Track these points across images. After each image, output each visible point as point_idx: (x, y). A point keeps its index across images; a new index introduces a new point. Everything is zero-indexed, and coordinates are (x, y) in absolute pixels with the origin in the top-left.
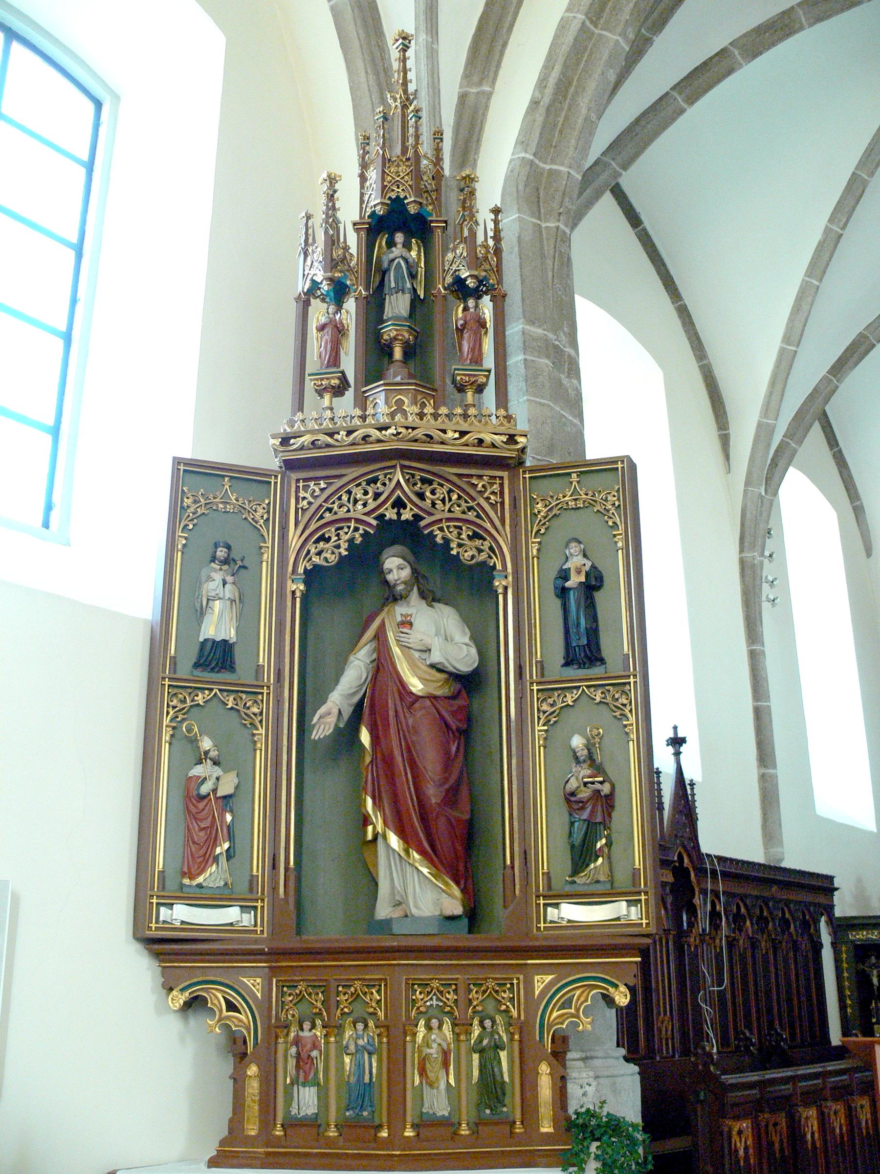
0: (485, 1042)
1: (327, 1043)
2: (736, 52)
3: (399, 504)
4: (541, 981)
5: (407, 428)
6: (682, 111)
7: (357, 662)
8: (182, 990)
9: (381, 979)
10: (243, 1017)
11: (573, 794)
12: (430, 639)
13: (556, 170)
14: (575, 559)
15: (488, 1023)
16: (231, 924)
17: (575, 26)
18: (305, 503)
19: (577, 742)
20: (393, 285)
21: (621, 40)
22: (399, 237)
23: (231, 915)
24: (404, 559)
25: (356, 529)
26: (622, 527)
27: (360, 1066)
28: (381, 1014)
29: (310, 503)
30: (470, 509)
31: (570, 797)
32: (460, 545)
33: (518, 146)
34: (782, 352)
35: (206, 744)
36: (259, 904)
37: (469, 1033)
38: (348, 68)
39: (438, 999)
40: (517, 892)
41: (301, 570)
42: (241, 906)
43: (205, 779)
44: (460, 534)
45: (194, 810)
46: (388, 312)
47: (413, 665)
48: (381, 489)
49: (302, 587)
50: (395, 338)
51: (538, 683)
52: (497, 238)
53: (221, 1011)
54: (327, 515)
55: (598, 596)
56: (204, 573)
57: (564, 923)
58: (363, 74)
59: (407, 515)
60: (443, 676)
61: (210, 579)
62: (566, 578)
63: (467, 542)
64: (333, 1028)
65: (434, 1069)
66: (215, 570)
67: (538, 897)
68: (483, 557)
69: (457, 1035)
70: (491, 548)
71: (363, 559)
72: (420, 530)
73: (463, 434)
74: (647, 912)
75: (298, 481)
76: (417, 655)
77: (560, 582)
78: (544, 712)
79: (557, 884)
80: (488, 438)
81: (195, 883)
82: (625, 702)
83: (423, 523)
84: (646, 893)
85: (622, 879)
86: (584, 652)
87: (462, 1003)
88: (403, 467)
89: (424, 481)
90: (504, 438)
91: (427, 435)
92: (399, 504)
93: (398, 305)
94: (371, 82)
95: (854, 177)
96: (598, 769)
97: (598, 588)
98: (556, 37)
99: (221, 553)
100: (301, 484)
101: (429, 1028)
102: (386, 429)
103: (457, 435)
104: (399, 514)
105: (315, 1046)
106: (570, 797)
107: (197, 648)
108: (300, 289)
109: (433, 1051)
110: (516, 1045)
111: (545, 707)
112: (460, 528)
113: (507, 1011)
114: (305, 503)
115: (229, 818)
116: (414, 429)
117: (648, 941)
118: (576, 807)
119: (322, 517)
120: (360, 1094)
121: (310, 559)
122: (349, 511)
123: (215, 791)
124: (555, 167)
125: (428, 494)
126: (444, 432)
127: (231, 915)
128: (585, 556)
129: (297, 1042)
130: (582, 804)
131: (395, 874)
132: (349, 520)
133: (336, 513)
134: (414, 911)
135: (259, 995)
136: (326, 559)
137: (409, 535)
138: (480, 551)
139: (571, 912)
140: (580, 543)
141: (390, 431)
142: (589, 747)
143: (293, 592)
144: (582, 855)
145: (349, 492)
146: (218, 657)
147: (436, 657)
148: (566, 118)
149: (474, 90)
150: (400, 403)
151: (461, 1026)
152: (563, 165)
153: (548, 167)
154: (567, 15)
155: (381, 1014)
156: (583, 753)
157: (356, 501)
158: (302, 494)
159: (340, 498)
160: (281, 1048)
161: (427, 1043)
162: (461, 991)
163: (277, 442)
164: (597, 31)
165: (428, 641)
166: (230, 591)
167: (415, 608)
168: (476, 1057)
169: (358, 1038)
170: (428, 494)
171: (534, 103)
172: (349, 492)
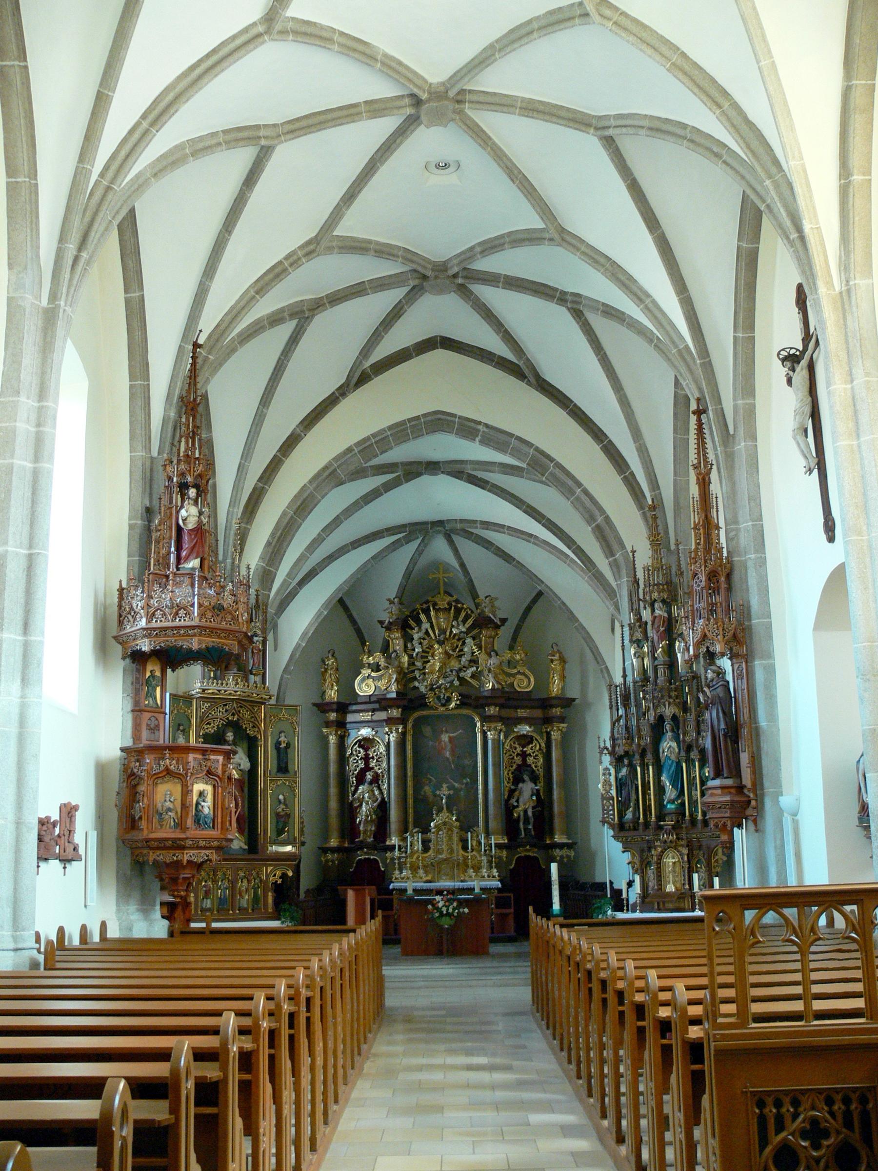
3: (233, 715)
4: (270, 869)
19: (281, 797)
27: (225, 893)
31: (278, 815)
52: (257, 600)
55: (289, 750)
64: (215, 881)
65: (243, 894)
80: (264, 696)
86: (283, 768)
92: (233, 715)
95: (337, 517)
99: (181, 728)
109: (244, 888)
120: (222, 901)
129: (204, 886)
130: (282, 816)
137: (235, 726)
139: (275, 848)
142: (285, 799)
144: (280, 832)
147: (242, 767)
151: (249, 881)
161: (241, 886)
165: (240, 761)
171: (268, 544)
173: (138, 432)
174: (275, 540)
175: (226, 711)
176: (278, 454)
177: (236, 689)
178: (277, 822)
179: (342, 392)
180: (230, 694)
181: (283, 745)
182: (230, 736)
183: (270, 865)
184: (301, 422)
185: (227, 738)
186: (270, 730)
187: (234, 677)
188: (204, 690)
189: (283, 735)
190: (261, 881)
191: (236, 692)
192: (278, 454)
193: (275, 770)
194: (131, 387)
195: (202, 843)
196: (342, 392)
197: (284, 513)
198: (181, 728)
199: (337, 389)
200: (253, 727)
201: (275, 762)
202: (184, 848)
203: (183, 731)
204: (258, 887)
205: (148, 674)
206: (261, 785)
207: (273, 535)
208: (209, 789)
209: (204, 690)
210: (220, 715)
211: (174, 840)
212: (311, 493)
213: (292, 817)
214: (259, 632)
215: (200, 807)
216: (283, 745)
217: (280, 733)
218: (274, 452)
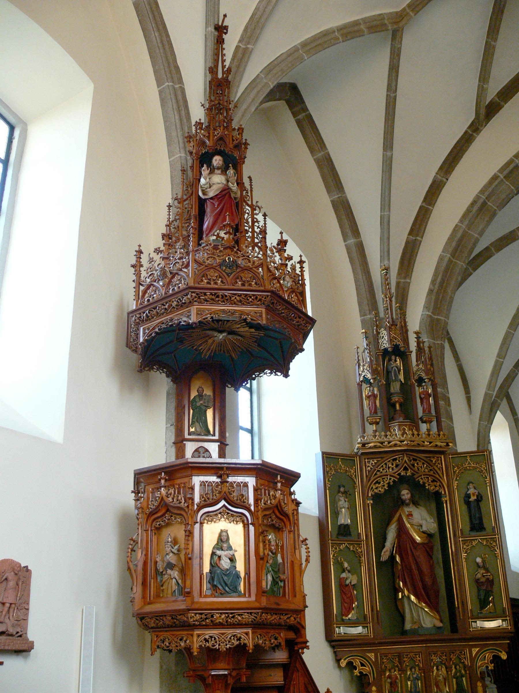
0: (458, 674)
1: (401, 677)
2: (493, 249)
3: (406, 469)
4: (475, 651)
5: (411, 441)
6: (471, 274)
7: (392, 530)
8: (345, 659)
9: (419, 652)
10: (367, 668)
11: (478, 579)
12: (419, 521)
13: (440, 319)
14: (471, 490)
15: (458, 667)
16: (360, 633)
17: (446, 259)
18: (369, 468)
19: (479, 560)
20: (394, 378)
21: (464, 265)
22: (393, 358)
23: (359, 630)
24: (408, 490)
25: (390, 479)
26: (488, 478)
27: (416, 686)
28: (421, 665)
29: (371, 468)
30: (431, 470)
32: (429, 485)
33: (425, 309)
34: (497, 362)
35: (346, 565)
36: (369, 625)
37: (451, 671)
38: (353, 271)
39: (440, 659)
40: (461, 617)
41: (370, 495)
42: (362, 626)
43: (347, 578)
44: (428, 480)
45: (344, 591)
46: (392, 390)
47: (416, 532)
48: (399, 463)
49: (372, 502)
50: (397, 401)
51: (462, 538)
53: (359, 667)
54: (378, 473)
55: (482, 504)
56: (337, 497)
57: (479, 629)
58: (361, 275)
59: (409, 474)
60: (426, 535)
61: (339, 500)
62: (470, 497)
63: (431, 483)
64: (402, 671)
65: (441, 685)
66: (341, 497)
67: (469, 619)
68: (437, 489)
69: (447, 672)
70: (440, 485)
71: (393, 489)
72: (414, 479)
73: (430, 443)
74: (510, 624)
75: (365, 459)
76: (416, 527)
77: (467, 499)
78: (465, 549)
79: (475, 614)
80: (439, 444)
81: (347, 618)
82: (495, 544)
83: (415, 476)
84: (509, 617)
85: (499, 611)
87: (448, 660)
88: (406, 454)
89: (414, 460)
90: (445, 444)
91: (418, 444)
92: (406, 469)
93: (395, 387)
94: (364, 279)
96: (487, 571)
97: (481, 501)
98: (438, 263)
99: (342, 489)
100: (366, 460)
101: (437, 669)
102: (403, 441)
103: (428, 443)
104: (406, 473)
105: (397, 678)
106: (477, 581)
107: (337, 528)
108: (358, 381)
109: (441, 678)
110: (468, 675)
111: (465, 547)
112: (428, 478)
113: (464, 662)
114: (369, 468)
115: (355, 592)
116: (413, 441)
117: (512, 635)
118: (481, 584)
119: (376, 474)
121: (373, 490)
122: (387, 472)
123: (351, 583)
124: (439, 317)
125: (416, 465)
126: (424, 442)
127: (359, 630)
128: (475, 488)
129: (389, 677)
131: (413, 611)
132: (387, 475)
133: (381, 472)
134: (424, 625)
135: (374, 660)
136: (380, 491)
138: (436, 486)
140: (473, 483)
141: (404, 443)
142: (483, 561)
143: (368, 504)
144: (483, 603)
145: (386, 464)
146: (344, 531)
147: (424, 528)
148: (443, 297)
149: (403, 281)
150: (404, 429)
152: (442, 316)
153: (436, 317)
154: (442, 254)
155: (421, 665)
156: (481, 564)
157: (389, 468)
158: (367, 465)
159: (382, 466)
160: (383, 680)
161: (438, 675)
162: (448, 655)
163: (360, 445)
164: (454, 260)
165: (421, 522)
166: (346, 505)
167: (412, 509)
168: (454, 680)
169: (413, 674)
170: (416, 465)
171: (431, 291)
172: (386, 464)
173: (174, 134)
174: (437, 286)
175: (397, 466)
176: (424, 204)
177: (402, 438)
178: (479, 590)
179: (475, 128)
180: (395, 445)
181: (473, 498)
182: (406, 494)
183: (475, 646)
184: (441, 168)
185: (403, 497)
186: (455, 484)
187: (400, 426)
188: (364, 445)
189: (471, 486)
190: (465, 667)
191: (402, 441)
192: (424, 204)
193: (467, 528)
194: (160, 92)
195: (219, 618)
196: (475, 128)
197: (441, 258)
198: (342, 489)
199: (469, 127)
200: (433, 481)
201: (467, 519)
202: (192, 627)
203: (345, 493)
204: (462, 676)
205: (194, 394)
206: (451, 548)
207: (433, 282)
208: (236, 532)
209: (364, 445)
210: (391, 471)
211: (174, 614)
212: (464, 231)
213: (496, 582)
214: (423, 375)
215: (216, 558)
216: (473, 498)
217: (468, 484)
218: (419, 203)
